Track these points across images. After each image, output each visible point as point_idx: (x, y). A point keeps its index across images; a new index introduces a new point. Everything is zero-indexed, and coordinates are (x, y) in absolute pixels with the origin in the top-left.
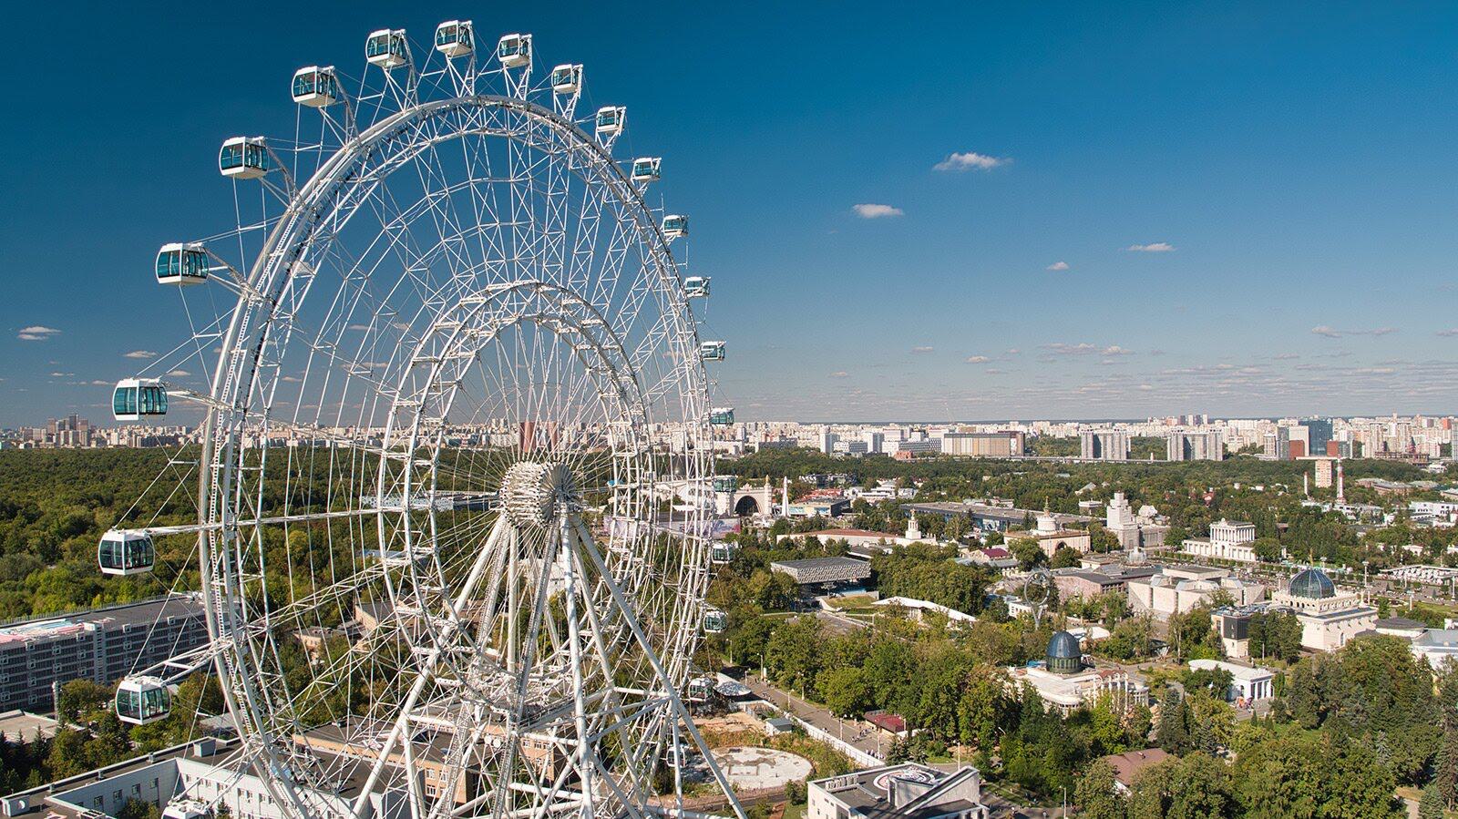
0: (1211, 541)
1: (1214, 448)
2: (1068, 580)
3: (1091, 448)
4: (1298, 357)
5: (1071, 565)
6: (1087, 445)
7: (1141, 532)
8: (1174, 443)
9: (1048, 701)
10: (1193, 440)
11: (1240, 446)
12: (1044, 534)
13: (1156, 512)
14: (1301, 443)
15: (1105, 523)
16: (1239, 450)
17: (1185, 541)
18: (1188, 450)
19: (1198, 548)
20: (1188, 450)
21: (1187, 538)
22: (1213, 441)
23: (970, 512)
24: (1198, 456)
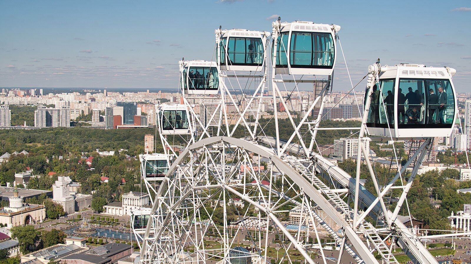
0: (123, 206)
1: (64, 119)
2: (72, 262)
3: (45, 119)
4: (67, 62)
5: (58, 243)
6: (42, 116)
7: (76, 203)
8: (40, 116)
9: (256, 155)
10: (52, 113)
11: (78, 116)
12: (15, 211)
13: (71, 180)
14: (119, 117)
15: (51, 195)
16: (77, 118)
17: (105, 206)
18: (49, 119)
19: (114, 210)
20: (49, 119)
21: (106, 204)
22: (64, 115)
23: (104, 156)
24: (55, 124)
